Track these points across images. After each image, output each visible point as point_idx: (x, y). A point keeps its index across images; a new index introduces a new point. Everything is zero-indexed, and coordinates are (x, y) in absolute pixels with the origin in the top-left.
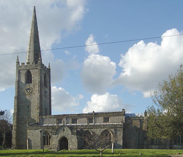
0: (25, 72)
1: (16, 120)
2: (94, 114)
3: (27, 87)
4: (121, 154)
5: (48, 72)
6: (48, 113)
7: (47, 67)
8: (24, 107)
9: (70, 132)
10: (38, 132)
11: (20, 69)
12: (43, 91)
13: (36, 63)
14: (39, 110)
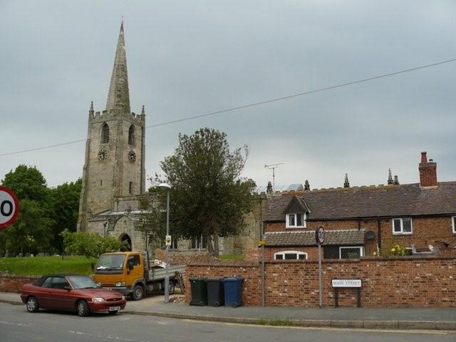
4: (83, 215)
10: (101, 224)
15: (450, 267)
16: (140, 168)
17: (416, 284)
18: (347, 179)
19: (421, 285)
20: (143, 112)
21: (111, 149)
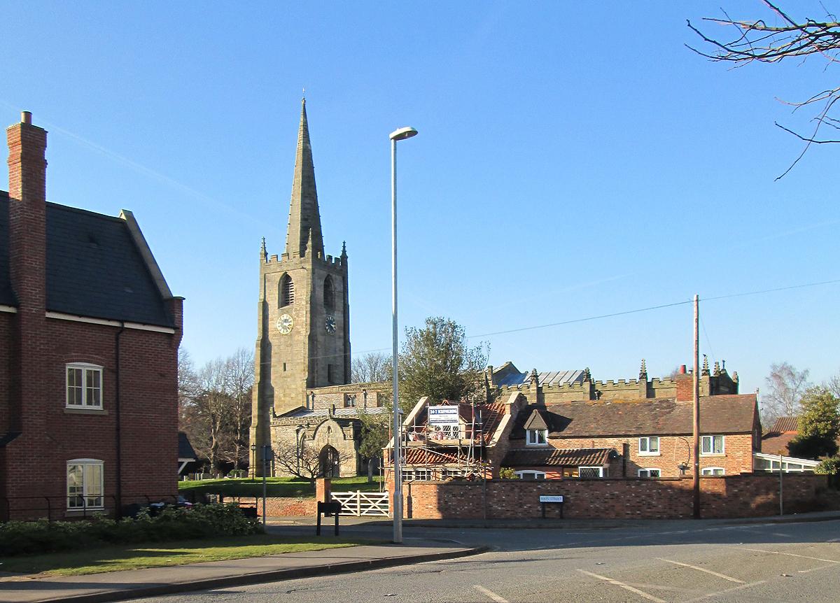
6: (339, 373)
9: (342, 435)
14: (307, 373)
15: (633, 487)
16: (342, 340)
17: (606, 500)
18: (643, 367)
19: (610, 501)
20: (344, 251)
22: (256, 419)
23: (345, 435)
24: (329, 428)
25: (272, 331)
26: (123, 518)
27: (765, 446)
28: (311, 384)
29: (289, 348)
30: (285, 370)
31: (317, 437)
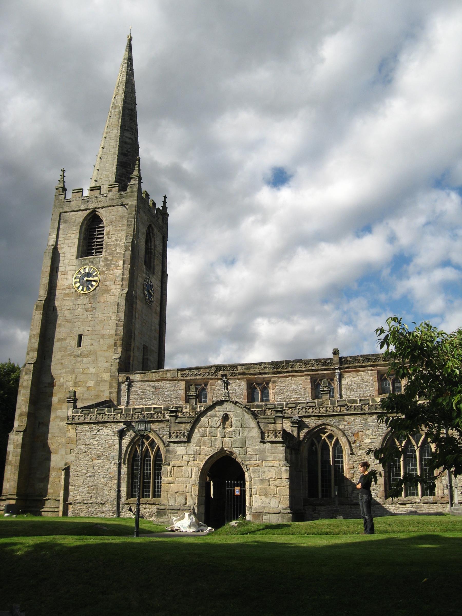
0: (80, 217)
1: (29, 391)
2: (336, 360)
3: (83, 290)
5: (160, 222)
6: (154, 357)
7: (159, 205)
8: (65, 339)
9: (255, 433)
10: (108, 434)
11: (66, 210)
12: (140, 281)
13: (123, 188)
14: (120, 350)
21: (108, 266)
22: (25, 419)
23: (263, 434)
24: (226, 418)
25: (64, 289)
26: (150, 203)
27: (375, 520)
28: (125, 366)
29: (91, 314)
30: (79, 345)
31: (196, 435)
